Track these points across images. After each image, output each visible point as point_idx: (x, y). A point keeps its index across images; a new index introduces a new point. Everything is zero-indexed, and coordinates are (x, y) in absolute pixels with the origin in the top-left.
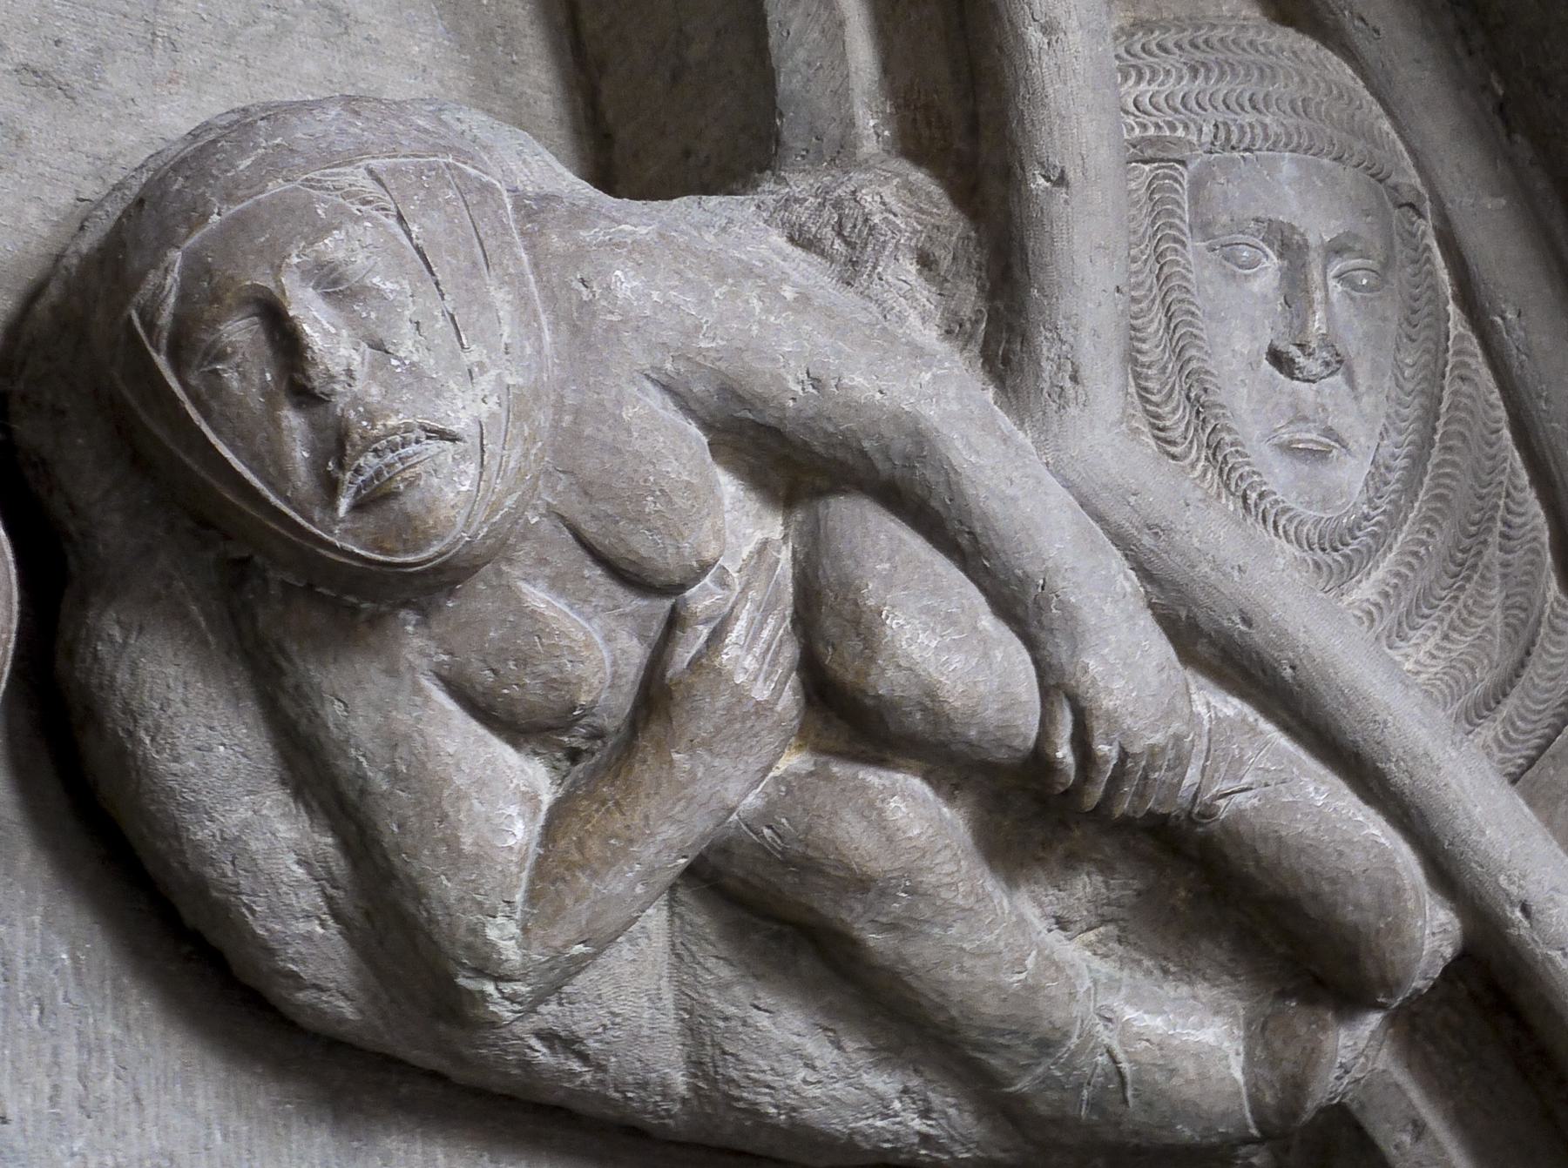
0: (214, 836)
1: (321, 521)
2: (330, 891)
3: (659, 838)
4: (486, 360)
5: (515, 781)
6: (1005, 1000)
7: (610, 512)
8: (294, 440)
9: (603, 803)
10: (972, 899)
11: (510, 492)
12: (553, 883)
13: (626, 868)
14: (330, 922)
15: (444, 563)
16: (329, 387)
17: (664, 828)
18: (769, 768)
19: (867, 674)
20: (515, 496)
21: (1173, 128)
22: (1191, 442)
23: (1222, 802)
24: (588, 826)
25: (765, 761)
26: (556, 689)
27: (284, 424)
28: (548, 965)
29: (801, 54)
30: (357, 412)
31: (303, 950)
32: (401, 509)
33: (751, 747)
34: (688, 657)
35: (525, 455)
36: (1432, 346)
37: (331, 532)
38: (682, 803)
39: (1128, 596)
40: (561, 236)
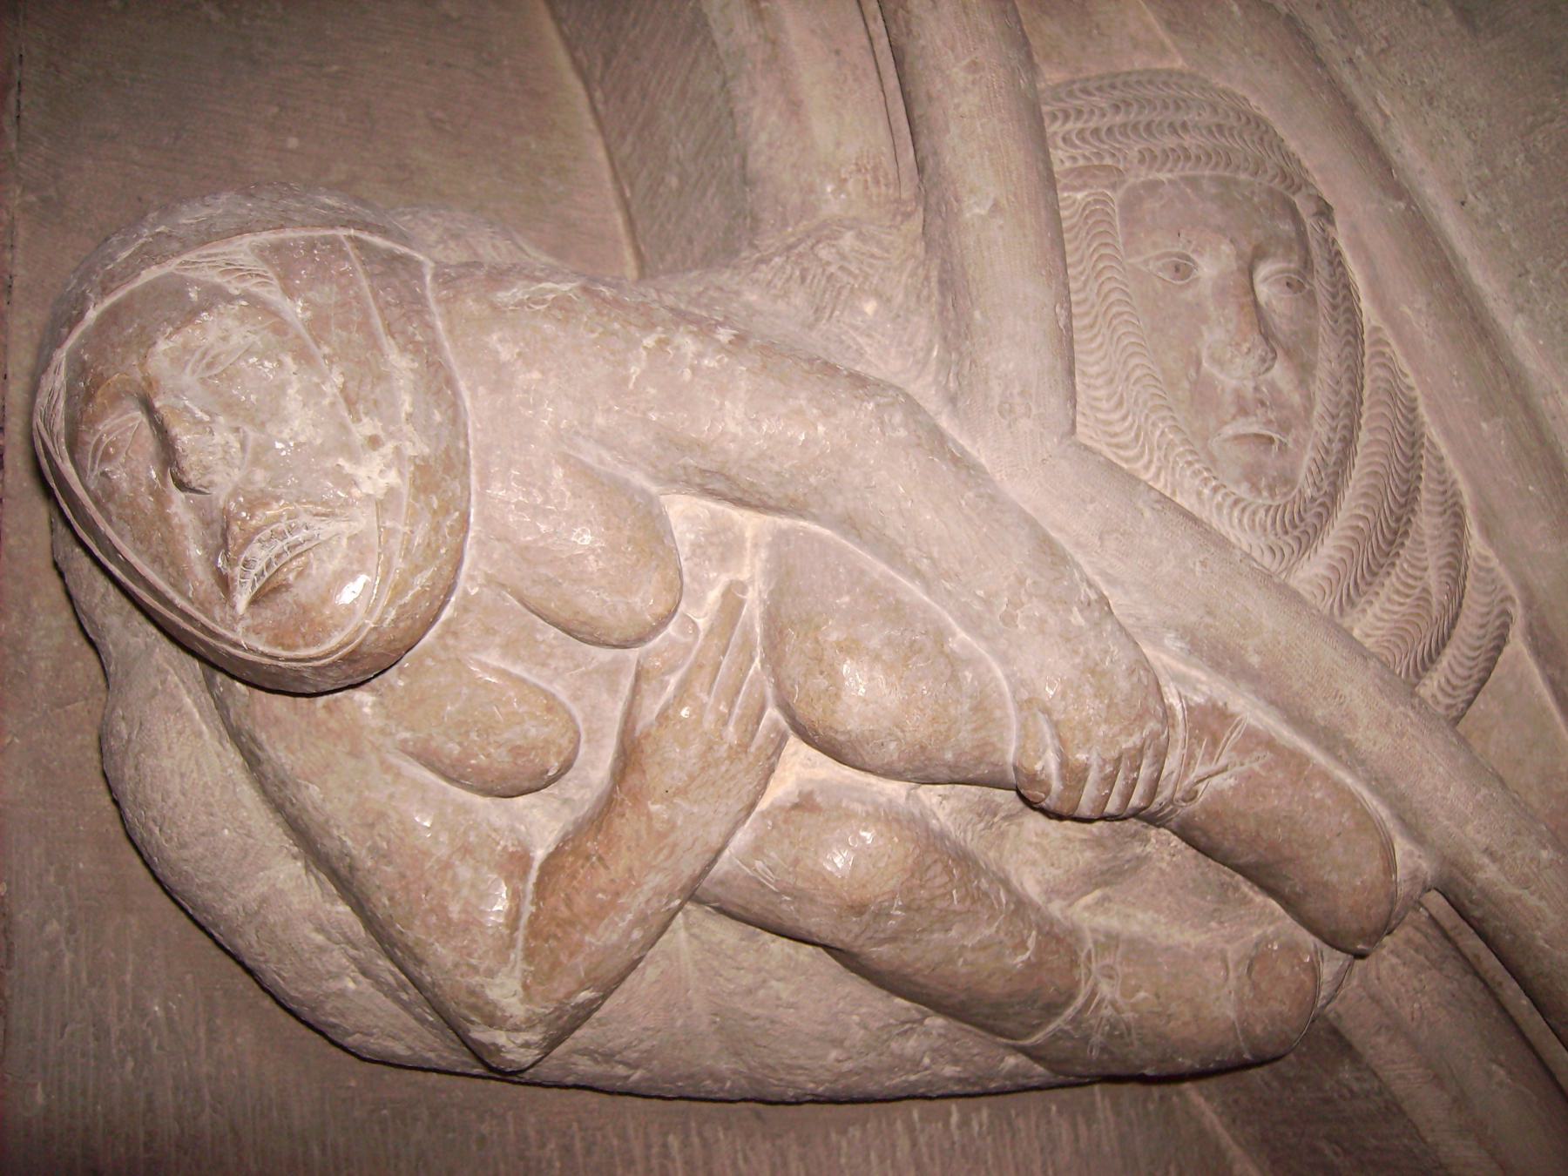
0: (237, 910)
1: (223, 620)
2: (353, 952)
3: (646, 887)
4: (382, 434)
5: (502, 843)
6: (1010, 980)
7: (551, 575)
8: (186, 538)
9: (588, 858)
10: (968, 903)
11: (418, 569)
12: (546, 940)
13: (616, 919)
14: (361, 978)
15: (353, 652)
16: (208, 478)
17: (651, 876)
18: (753, 805)
19: (833, 712)
20: (428, 573)
21: (1099, 155)
22: (1143, 445)
23: (1202, 786)
24: (575, 883)
25: (747, 801)
26: (524, 755)
27: (176, 521)
28: (552, 1016)
29: (763, 137)
30: (237, 502)
31: (339, 1005)
32: (295, 602)
33: (729, 790)
34: (657, 708)
35: (436, 528)
36: (1351, 339)
37: (234, 630)
38: (665, 852)
39: (1093, 604)
40: (477, 300)
